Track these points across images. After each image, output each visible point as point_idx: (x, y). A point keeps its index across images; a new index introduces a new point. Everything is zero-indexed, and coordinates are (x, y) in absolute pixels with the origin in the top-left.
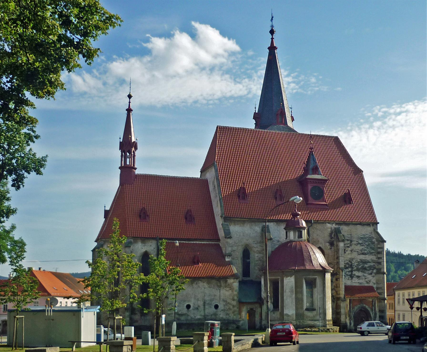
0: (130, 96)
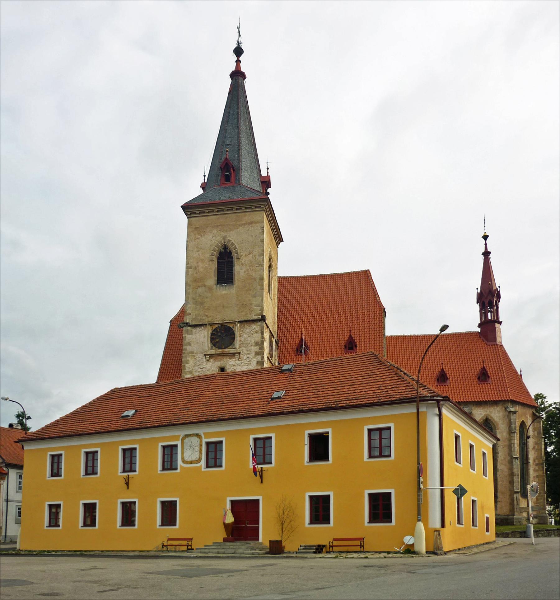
0: (485, 237)
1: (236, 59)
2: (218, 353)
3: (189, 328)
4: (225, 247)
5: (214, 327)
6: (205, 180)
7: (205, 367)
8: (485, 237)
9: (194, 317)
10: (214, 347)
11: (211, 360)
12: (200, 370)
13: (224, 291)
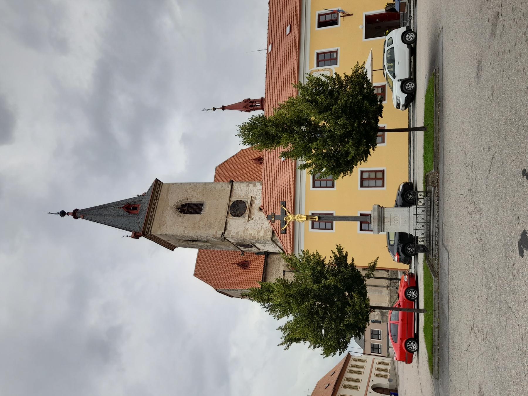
0: (214, 109)
1: (67, 215)
2: (248, 211)
3: (226, 233)
4: (178, 208)
5: (230, 214)
6: (130, 236)
7: (256, 222)
8: (214, 109)
9: (219, 229)
10: (243, 215)
11: (253, 217)
12: (258, 226)
13: (206, 210)
